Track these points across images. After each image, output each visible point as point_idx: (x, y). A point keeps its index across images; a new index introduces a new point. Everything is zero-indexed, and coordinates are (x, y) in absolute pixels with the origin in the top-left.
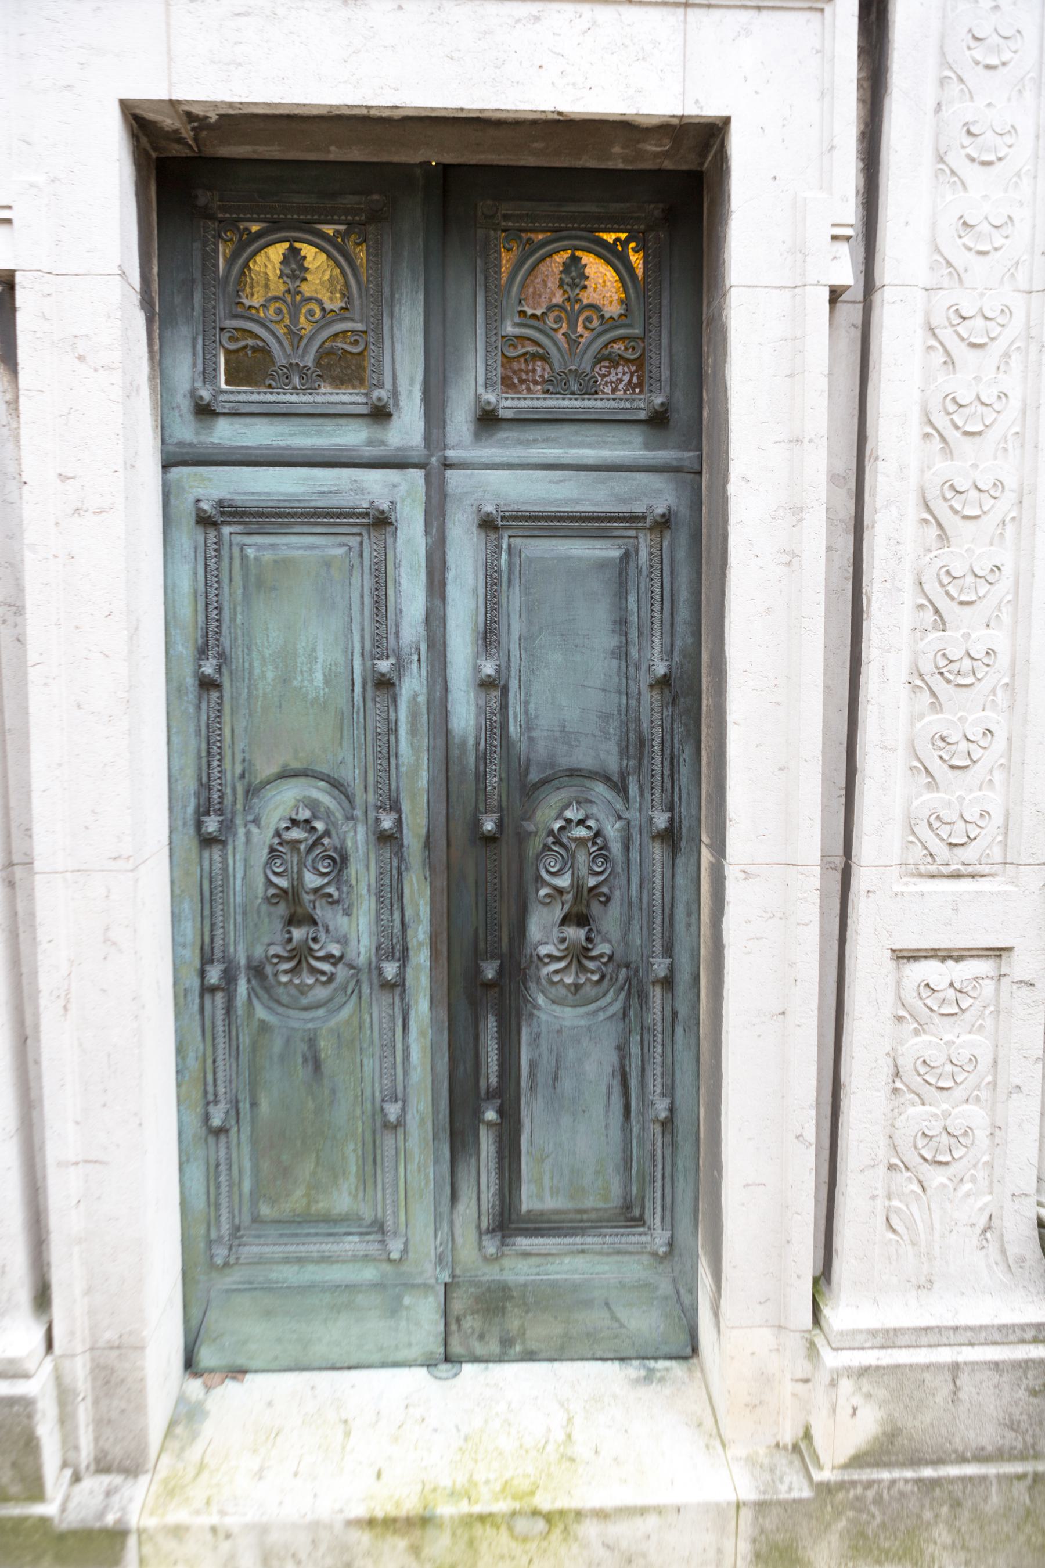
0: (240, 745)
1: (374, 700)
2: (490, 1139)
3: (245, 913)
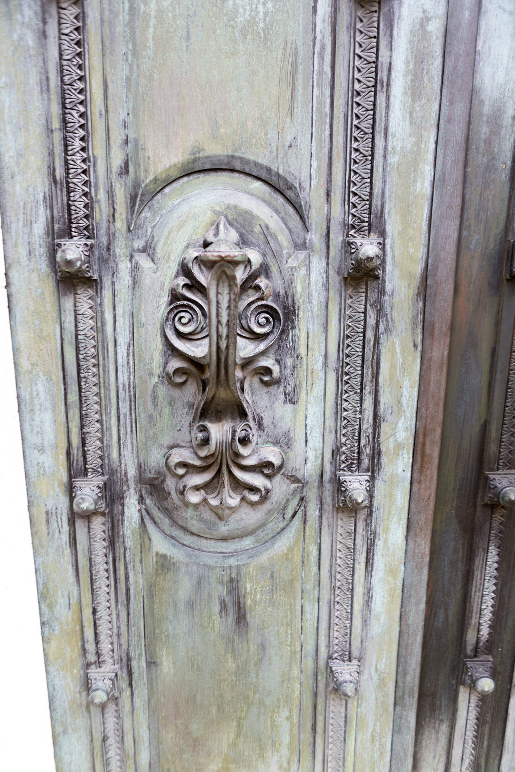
0: (119, 114)
1: (353, 29)
2: (473, 705)
3: (133, 399)
